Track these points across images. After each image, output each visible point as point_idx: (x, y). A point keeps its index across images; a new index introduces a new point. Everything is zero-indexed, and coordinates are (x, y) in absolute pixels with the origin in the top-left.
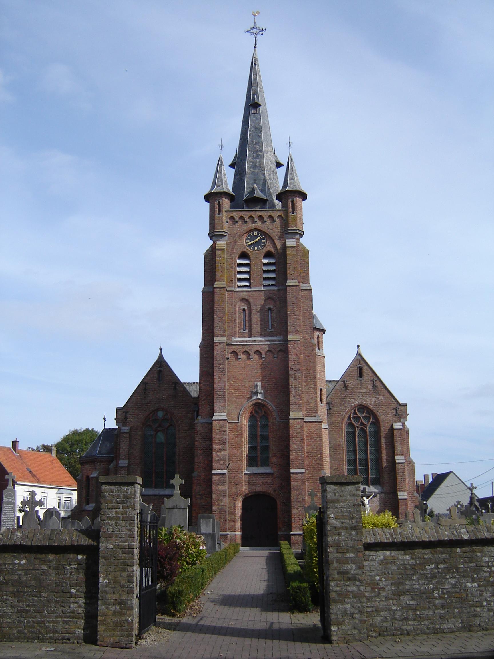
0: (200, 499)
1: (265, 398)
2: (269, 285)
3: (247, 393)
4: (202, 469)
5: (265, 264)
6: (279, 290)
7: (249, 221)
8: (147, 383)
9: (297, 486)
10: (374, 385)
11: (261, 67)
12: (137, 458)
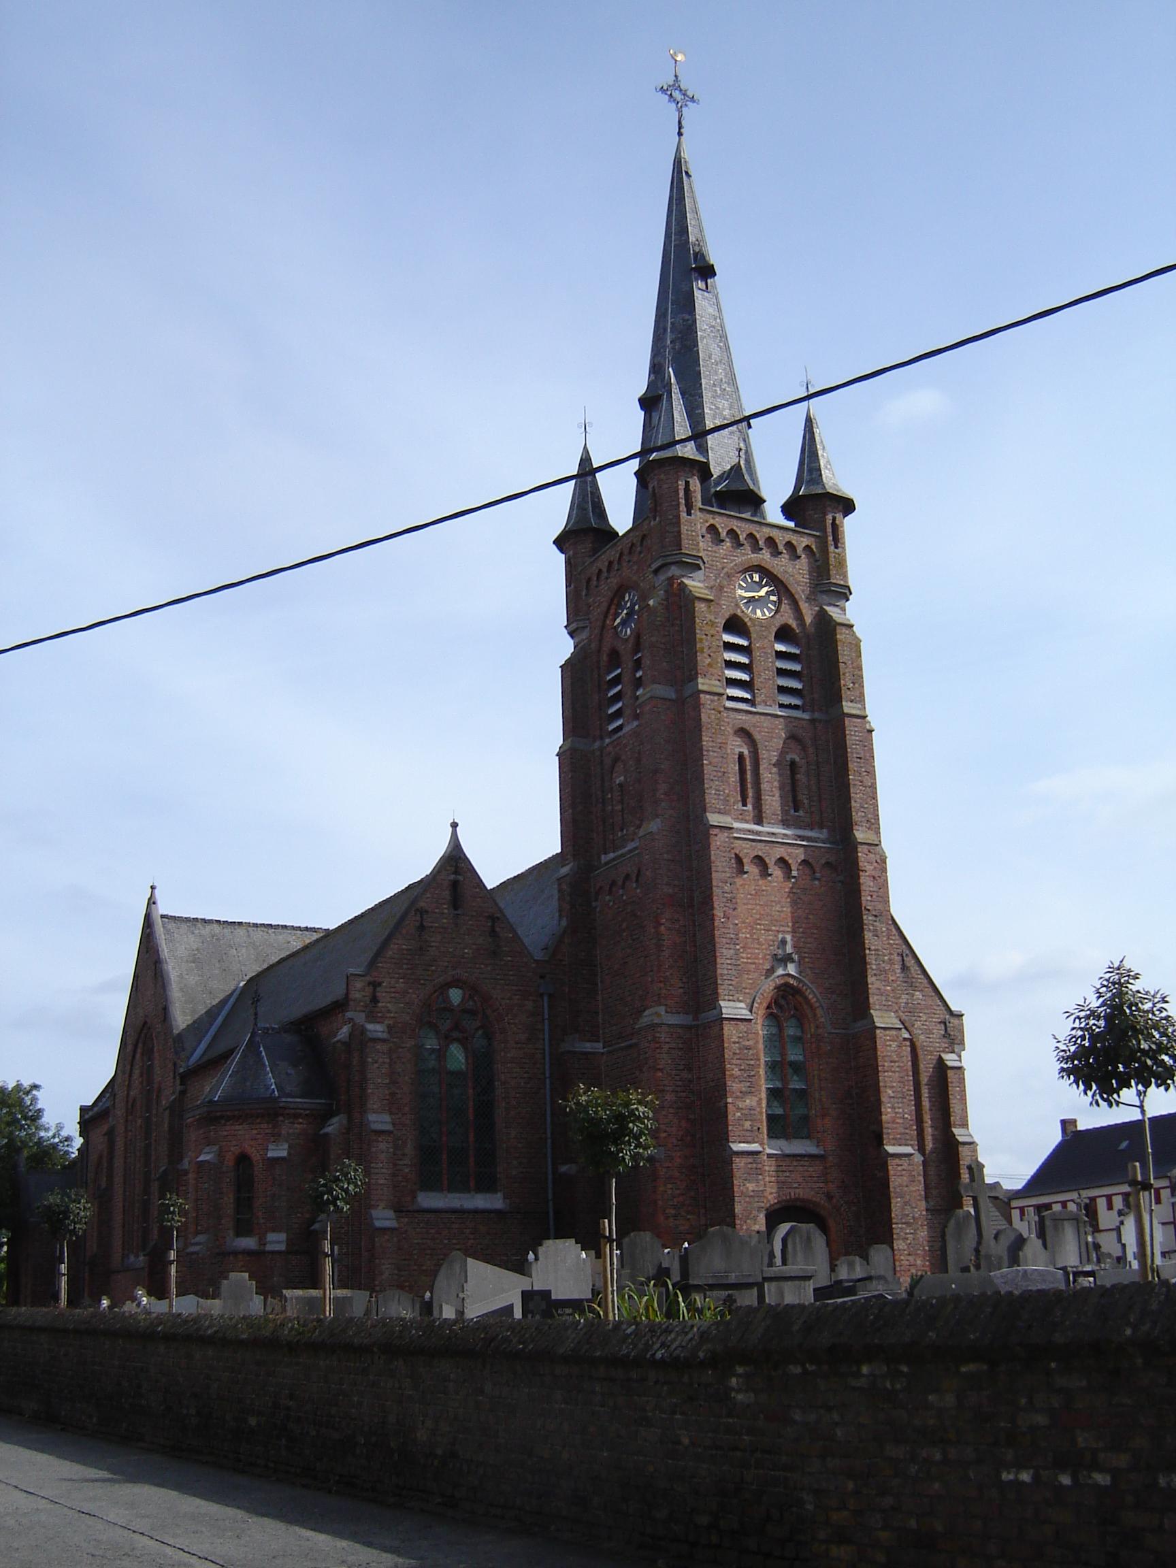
0: (675, 1216)
1: (800, 973)
2: (789, 706)
3: (764, 958)
4: (675, 1141)
5: (780, 655)
6: (812, 721)
7: (747, 547)
8: (427, 912)
9: (901, 1185)
10: (903, 964)
11: (701, 190)
12: (407, 1109)
